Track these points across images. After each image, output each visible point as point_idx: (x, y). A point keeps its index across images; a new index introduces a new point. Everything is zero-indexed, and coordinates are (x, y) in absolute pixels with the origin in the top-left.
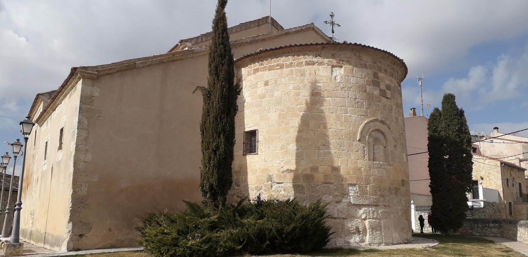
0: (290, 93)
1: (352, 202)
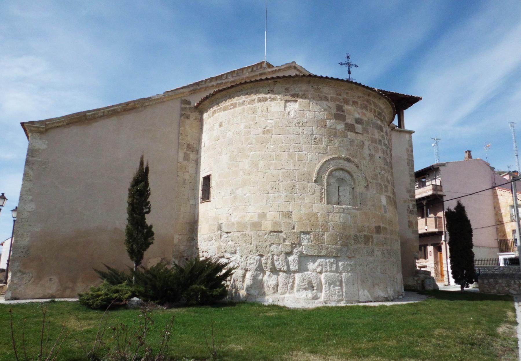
1: (304, 252)
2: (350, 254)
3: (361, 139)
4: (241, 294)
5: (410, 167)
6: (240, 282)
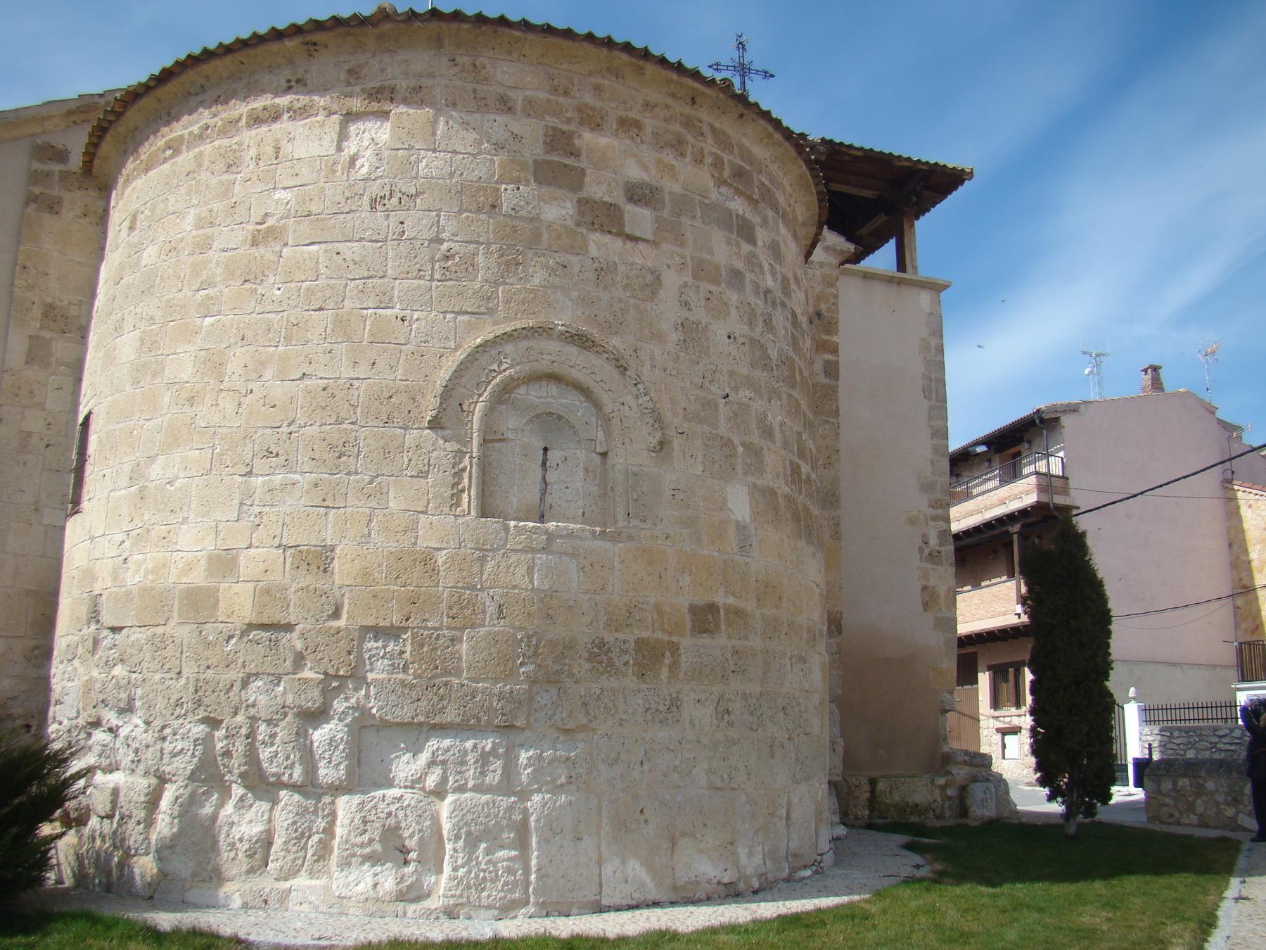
0: (183, 245)
1: (374, 711)
2: (570, 716)
3: (649, 264)
4: (137, 871)
5: (933, 403)
6: (139, 823)
